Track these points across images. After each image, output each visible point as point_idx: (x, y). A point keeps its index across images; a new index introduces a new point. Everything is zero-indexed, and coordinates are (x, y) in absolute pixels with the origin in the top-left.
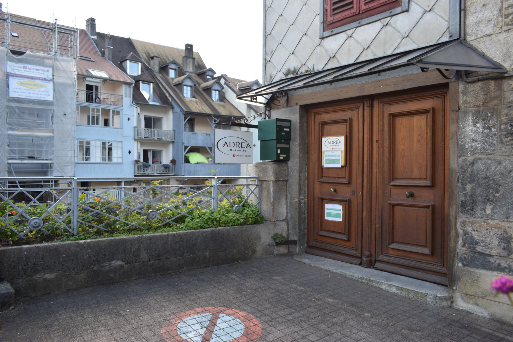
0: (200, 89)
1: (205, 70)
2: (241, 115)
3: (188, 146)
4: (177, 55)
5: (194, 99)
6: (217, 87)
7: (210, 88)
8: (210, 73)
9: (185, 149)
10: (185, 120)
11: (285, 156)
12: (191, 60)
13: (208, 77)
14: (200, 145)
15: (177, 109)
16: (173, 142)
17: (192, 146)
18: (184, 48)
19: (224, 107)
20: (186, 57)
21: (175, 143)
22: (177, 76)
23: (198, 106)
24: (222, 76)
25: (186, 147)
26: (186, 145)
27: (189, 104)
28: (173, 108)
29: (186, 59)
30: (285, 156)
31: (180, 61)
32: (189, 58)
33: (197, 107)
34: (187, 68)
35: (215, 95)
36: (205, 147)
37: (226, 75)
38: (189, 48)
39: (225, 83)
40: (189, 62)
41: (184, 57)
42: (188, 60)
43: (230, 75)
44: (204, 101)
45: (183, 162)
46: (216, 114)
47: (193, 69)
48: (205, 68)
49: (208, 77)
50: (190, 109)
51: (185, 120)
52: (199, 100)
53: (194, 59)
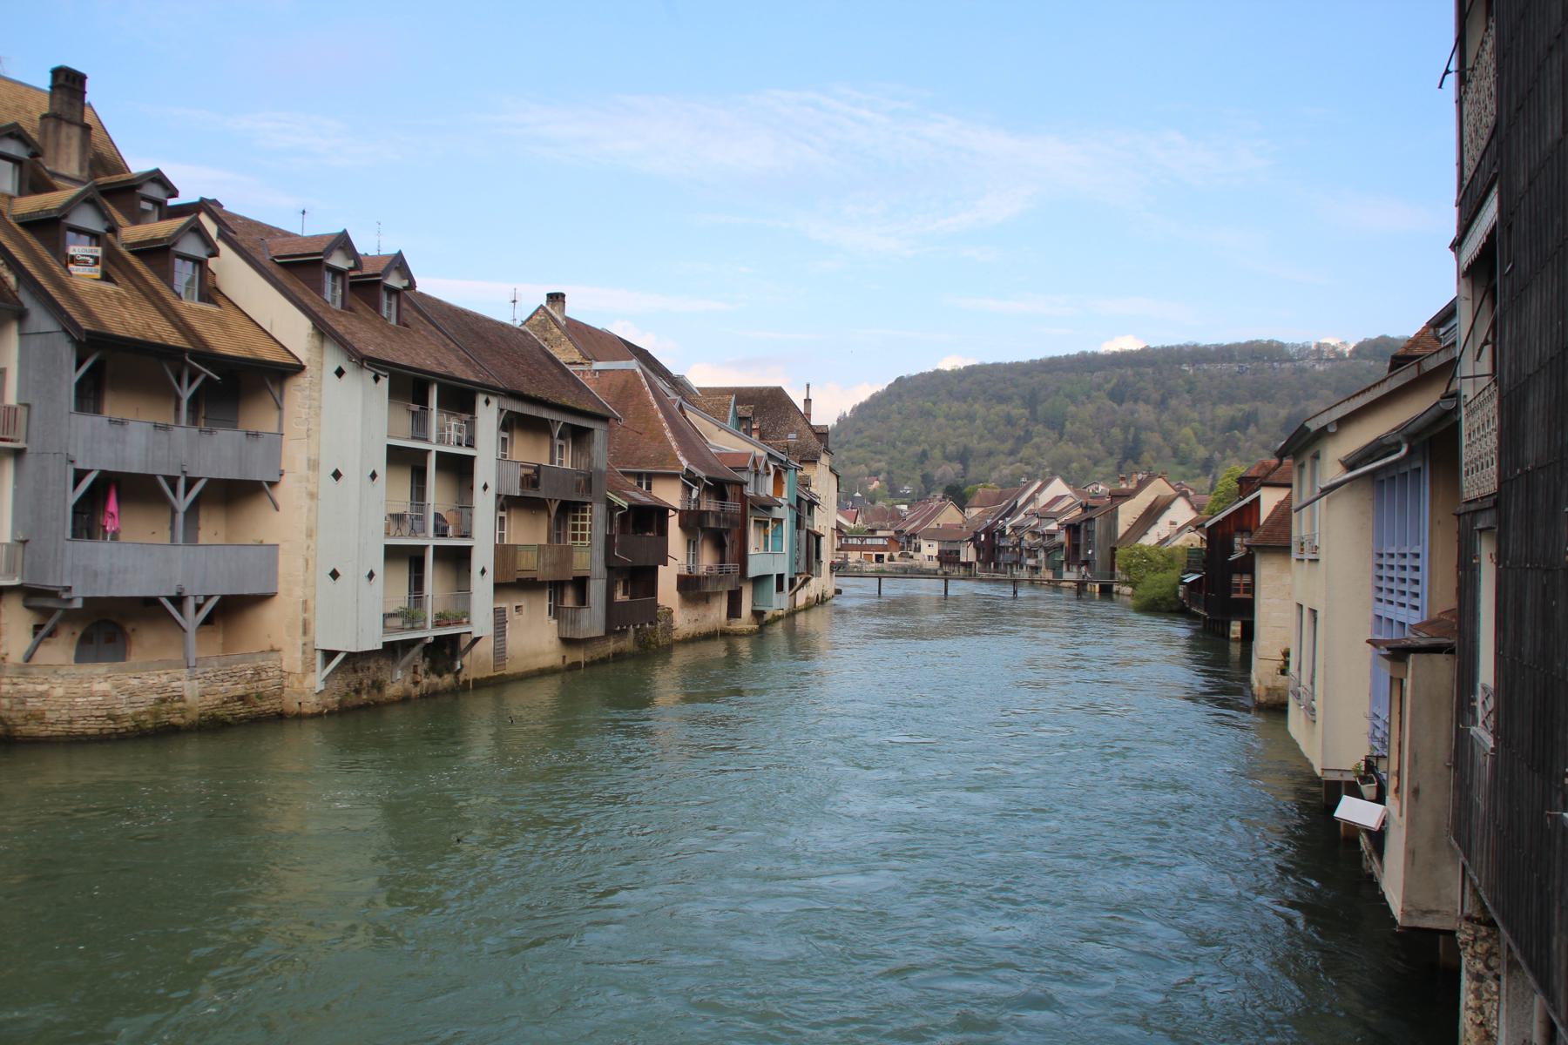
0: (122, 250)
1: (124, 177)
2: (291, 361)
3: (88, 472)
4: (10, 104)
5: (108, 287)
6: (192, 246)
7: (166, 249)
8: (154, 191)
9: (76, 484)
10: (78, 367)
11: (1233, 558)
12: (76, 132)
13: (146, 205)
14: (135, 470)
15: (40, 320)
16: (18, 454)
17: (103, 473)
18: (45, 83)
19: (222, 325)
20: (54, 118)
21: (29, 461)
22: (26, 187)
23: (129, 318)
24: (205, 206)
25: (79, 475)
26: (80, 466)
27: (96, 306)
28: (21, 316)
29: (57, 127)
30: (1233, 558)
31: (31, 127)
32: (70, 123)
33: (127, 316)
34: (56, 161)
35: (184, 273)
36: (153, 477)
37: (215, 202)
38: (69, 83)
39: (221, 235)
40: (69, 138)
41: (44, 117)
42: (65, 129)
43: (231, 206)
44: (147, 297)
45: (69, 535)
46: (201, 348)
47: (81, 169)
48: (121, 167)
49: (146, 205)
50: (103, 325)
51: (78, 367)
52: (127, 289)
53: (87, 129)
